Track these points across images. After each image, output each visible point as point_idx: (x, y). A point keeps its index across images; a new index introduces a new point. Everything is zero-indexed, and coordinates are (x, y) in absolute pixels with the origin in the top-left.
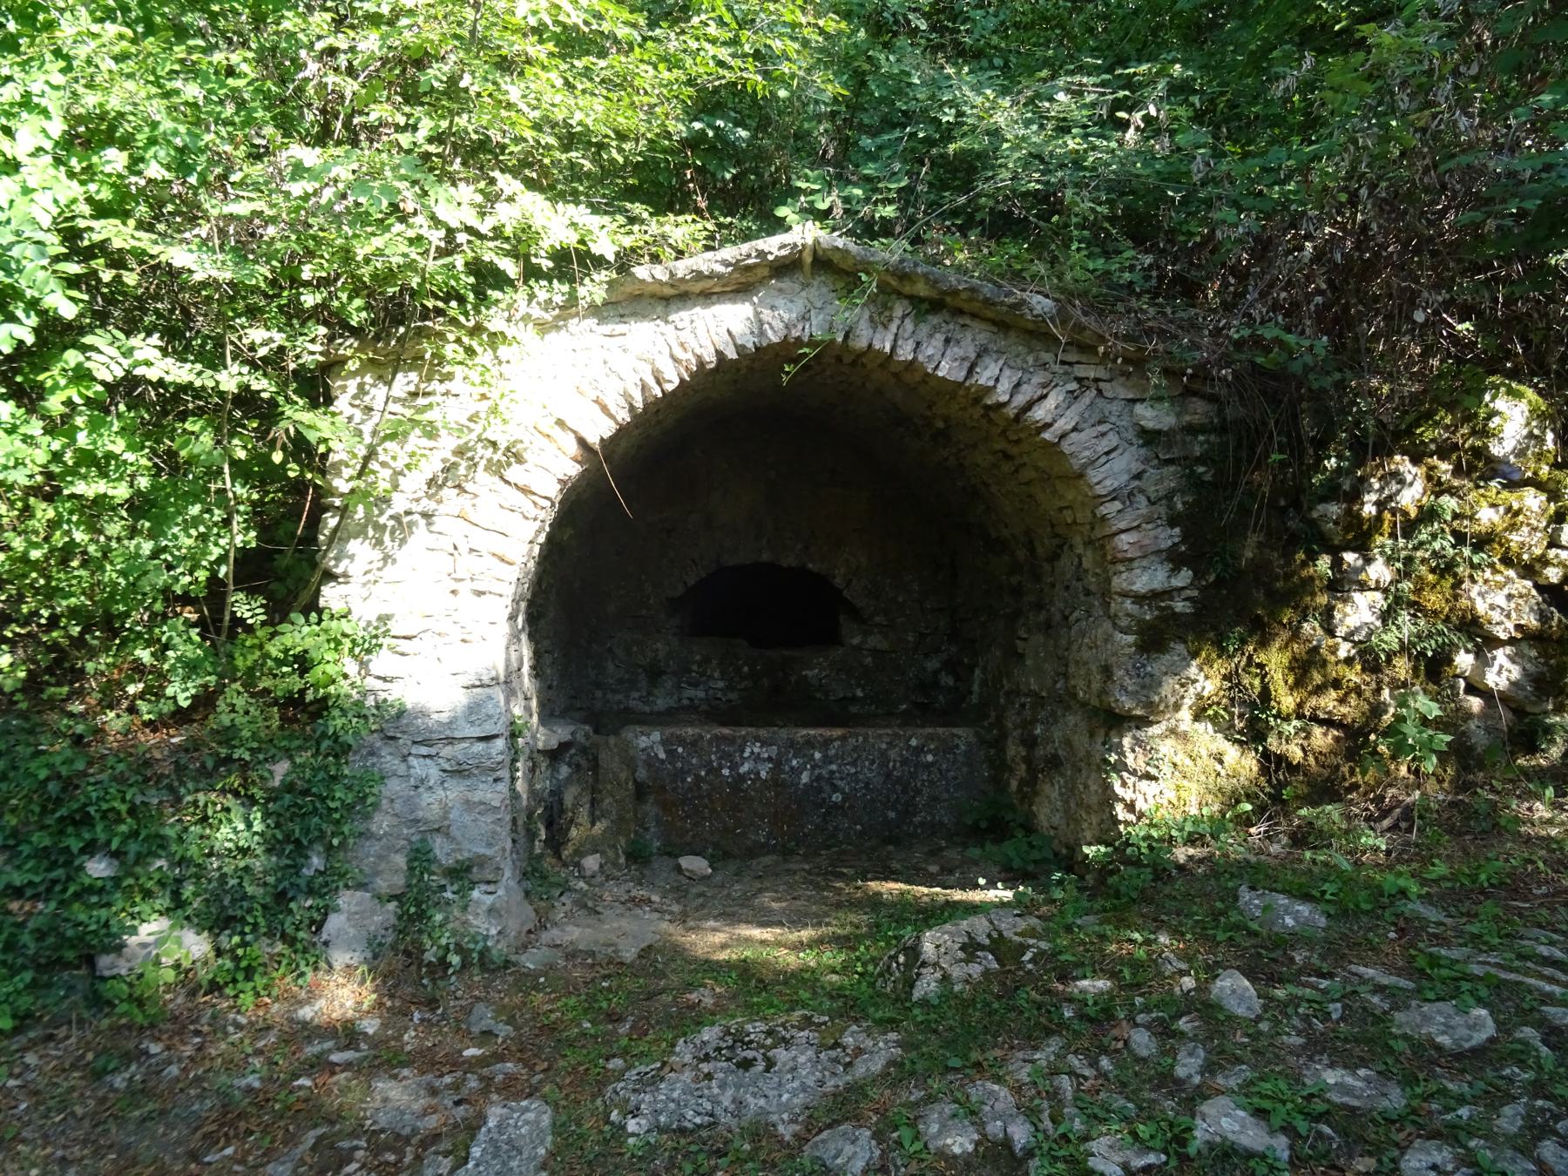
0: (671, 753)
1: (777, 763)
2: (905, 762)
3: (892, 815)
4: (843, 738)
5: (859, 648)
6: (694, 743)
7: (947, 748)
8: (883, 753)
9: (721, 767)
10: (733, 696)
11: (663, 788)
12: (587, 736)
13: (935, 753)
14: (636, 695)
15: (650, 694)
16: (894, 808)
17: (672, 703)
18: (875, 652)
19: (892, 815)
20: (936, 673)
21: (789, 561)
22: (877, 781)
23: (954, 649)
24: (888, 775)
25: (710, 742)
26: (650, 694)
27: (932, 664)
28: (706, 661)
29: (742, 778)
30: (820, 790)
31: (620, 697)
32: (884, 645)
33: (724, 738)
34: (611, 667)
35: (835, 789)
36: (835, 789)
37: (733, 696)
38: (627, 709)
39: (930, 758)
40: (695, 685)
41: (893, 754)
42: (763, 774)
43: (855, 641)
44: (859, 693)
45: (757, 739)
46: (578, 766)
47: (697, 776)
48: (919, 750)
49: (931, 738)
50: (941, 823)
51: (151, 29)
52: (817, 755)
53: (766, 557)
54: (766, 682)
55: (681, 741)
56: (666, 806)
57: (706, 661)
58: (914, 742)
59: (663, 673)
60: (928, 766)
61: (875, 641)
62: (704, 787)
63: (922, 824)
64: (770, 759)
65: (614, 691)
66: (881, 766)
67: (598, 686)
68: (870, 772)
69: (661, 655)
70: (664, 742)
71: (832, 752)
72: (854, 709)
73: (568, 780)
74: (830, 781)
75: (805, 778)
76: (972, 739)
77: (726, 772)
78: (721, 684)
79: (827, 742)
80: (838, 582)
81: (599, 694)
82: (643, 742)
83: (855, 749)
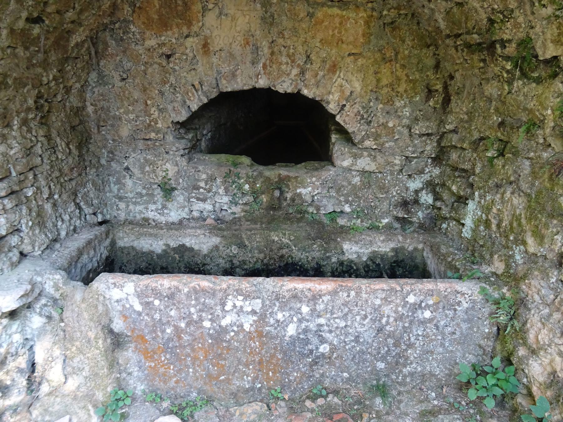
0: (147, 305)
1: (262, 317)
2: (400, 318)
3: (381, 365)
4: (334, 293)
5: (349, 170)
6: (171, 296)
7: (447, 304)
8: (377, 309)
9: (201, 319)
10: (237, 209)
11: (142, 338)
12: (57, 288)
13: (434, 308)
14: (153, 207)
15: (164, 207)
16: (383, 359)
17: (184, 214)
18: (363, 172)
19: (381, 365)
20: (417, 192)
21: (285, 87)
22: (368, 335)
23: (437, 171)
24: (380, 330)
25: (188, 296)
26: (164, 207)
27: (415, 184)
28: (212, 179)
29: (224, 330)
30: (307, 342)
31: (139, 208)
32: (372, 167)
33: (204, 290)
34: (129, 183)
35: (323, 341)
36: (323, 341)
37: (237, 209)
38: (146, 220)
39: (427, 314)
40: (204, 200)
41: (387, 310)
42: (247, 327)
43: (346, 164)
44: (347, 209)
45: (239, 292)
46: (49, 318)
47: (176, 328)
48: (417, 307)
49: (430, 293)
50: (432, 374)
51: (522, 231)
52: (305, 309)
53: (262, 83)
54: (264, 198)
55: (157, 294)
56: (148, 355)
57: (212, 179)
58: (411, 299)
59: (173, 189)
60: (423, 322)
61: (365, 163)
62: (186, 338)
63: (411, 374)
64: (254, 312)
65: (135, 203)
66: (373, 321)
67: (121, 199)
68: (364, 328)
69: (170, 174)
70: (140, 295)
71: (320, 307)
72: (342, 221)
73: (42, 332)
74: (318, 333)
75: (291, 330)
76: (478, 297)
77: (207, 324)
78: (226, 199)
79: (315, 298)
80: (332, 108)
81: (122, 205)
82: (116, 294)
83: (345, 304)
